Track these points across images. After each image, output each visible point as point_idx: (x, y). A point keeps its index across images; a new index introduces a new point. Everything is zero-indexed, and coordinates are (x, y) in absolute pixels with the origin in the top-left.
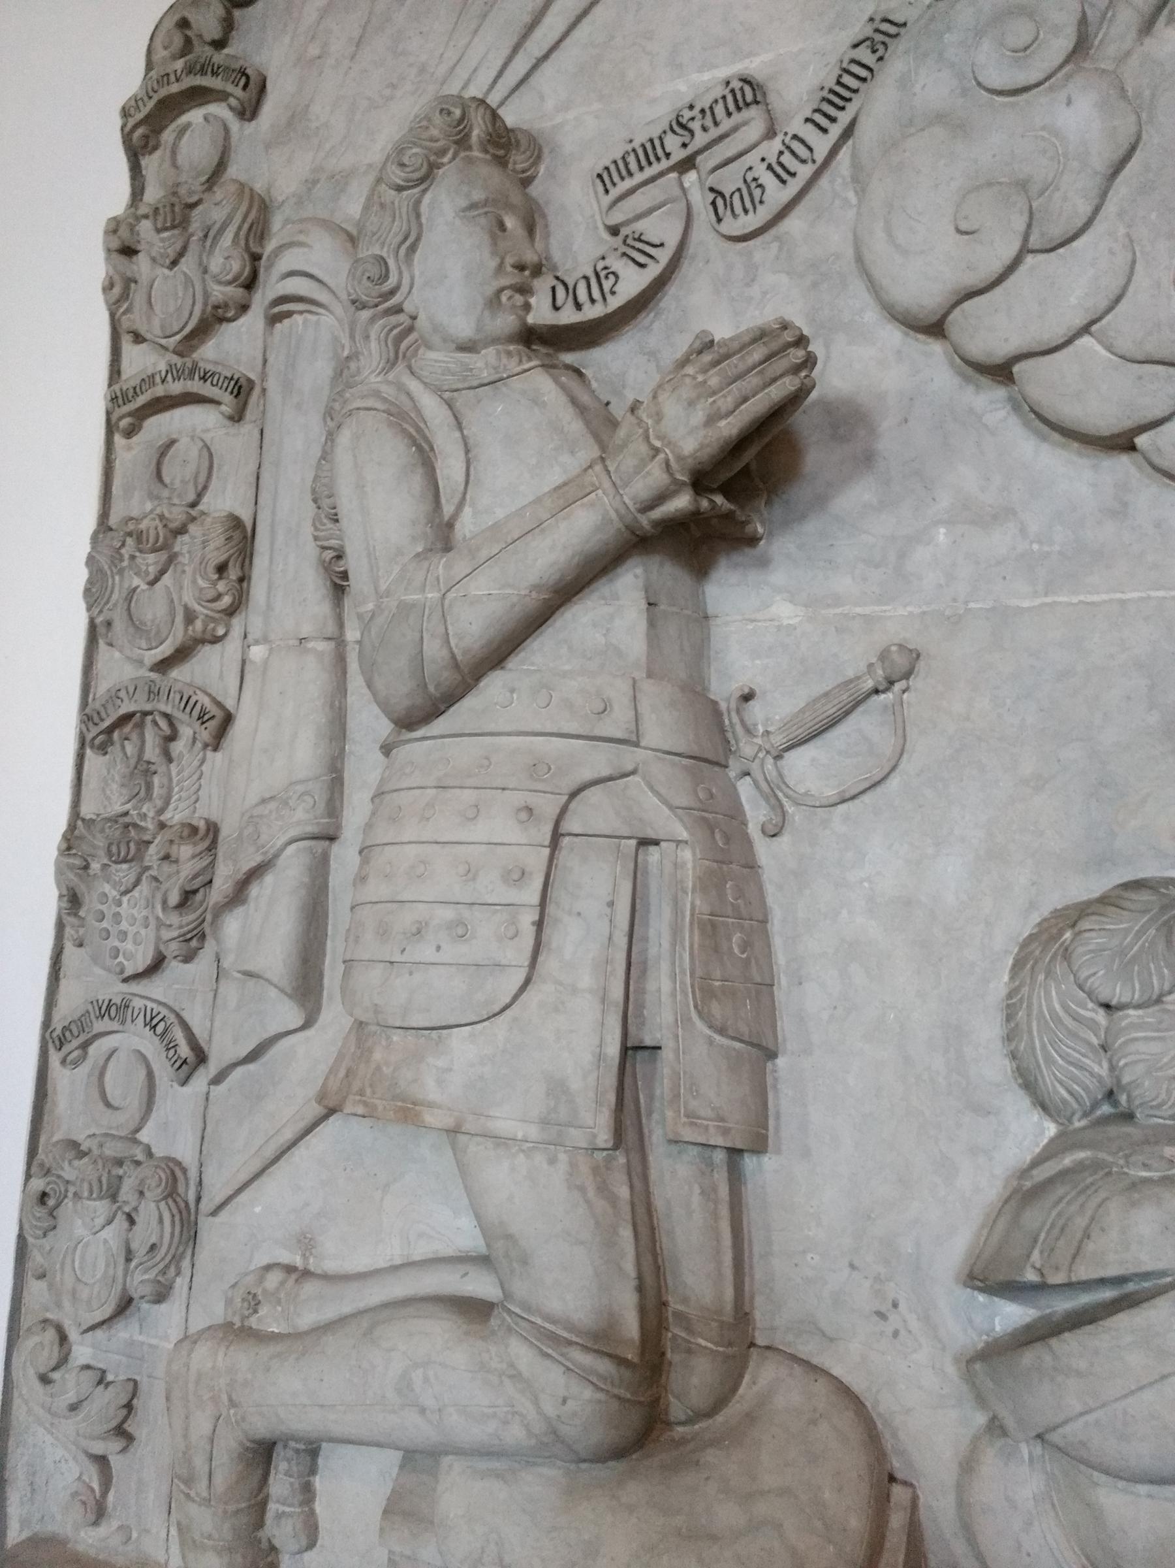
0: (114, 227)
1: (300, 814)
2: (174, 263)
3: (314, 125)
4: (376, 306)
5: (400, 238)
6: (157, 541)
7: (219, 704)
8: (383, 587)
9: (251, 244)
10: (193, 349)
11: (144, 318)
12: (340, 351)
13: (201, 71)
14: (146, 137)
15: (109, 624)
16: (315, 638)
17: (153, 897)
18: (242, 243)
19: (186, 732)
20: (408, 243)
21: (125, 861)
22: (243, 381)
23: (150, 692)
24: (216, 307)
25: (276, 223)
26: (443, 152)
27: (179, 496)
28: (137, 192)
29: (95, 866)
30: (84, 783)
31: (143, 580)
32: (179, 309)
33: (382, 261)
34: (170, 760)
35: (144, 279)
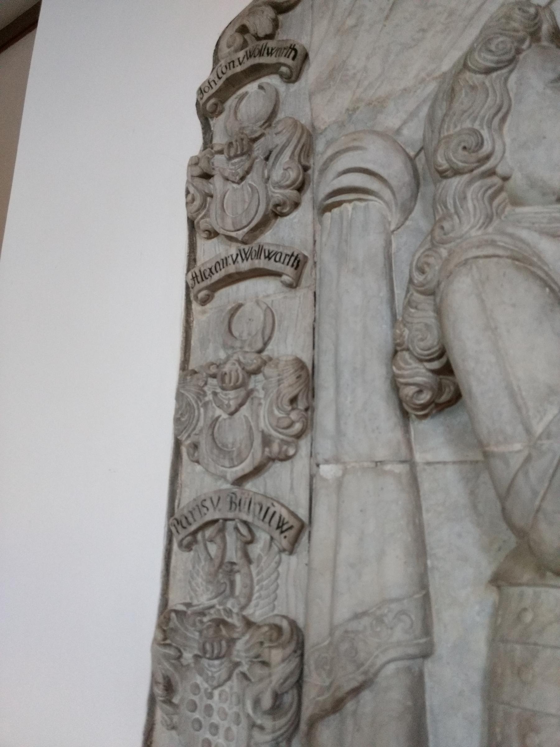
0: (195, 162)
1: (398, 634)
2: (242, 179)
3: (351, 73)
4: (472, 171)
5: (493, 111)
6: (237, 381)
7: (293, 514)
8: (538, 428)
9: (302, 160)
10: (256, 238)
11: (219, 220)
12: (387, 226)
13: (258, 52)
14: (216, 105)
15: (195, 446)
16: (391, 462)
17: (244, 695)
18: (296, 158)
19: (263, 537)
20: (500, 115)
21: (218, 658)
22: (300, 257)
23: (231, 502)
24: (277, 205)
25: (320, 146)
26: (522, 41)
27: (250, 345)
28: (208, 142)
29: (188, 656)
30: (171, 574)
31: (225, 411)
32: (247, 211)
33: (476, 132)
34: (250, 562)
35: (218, 195)
